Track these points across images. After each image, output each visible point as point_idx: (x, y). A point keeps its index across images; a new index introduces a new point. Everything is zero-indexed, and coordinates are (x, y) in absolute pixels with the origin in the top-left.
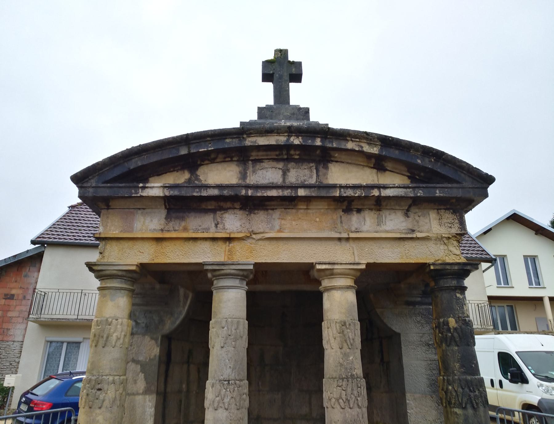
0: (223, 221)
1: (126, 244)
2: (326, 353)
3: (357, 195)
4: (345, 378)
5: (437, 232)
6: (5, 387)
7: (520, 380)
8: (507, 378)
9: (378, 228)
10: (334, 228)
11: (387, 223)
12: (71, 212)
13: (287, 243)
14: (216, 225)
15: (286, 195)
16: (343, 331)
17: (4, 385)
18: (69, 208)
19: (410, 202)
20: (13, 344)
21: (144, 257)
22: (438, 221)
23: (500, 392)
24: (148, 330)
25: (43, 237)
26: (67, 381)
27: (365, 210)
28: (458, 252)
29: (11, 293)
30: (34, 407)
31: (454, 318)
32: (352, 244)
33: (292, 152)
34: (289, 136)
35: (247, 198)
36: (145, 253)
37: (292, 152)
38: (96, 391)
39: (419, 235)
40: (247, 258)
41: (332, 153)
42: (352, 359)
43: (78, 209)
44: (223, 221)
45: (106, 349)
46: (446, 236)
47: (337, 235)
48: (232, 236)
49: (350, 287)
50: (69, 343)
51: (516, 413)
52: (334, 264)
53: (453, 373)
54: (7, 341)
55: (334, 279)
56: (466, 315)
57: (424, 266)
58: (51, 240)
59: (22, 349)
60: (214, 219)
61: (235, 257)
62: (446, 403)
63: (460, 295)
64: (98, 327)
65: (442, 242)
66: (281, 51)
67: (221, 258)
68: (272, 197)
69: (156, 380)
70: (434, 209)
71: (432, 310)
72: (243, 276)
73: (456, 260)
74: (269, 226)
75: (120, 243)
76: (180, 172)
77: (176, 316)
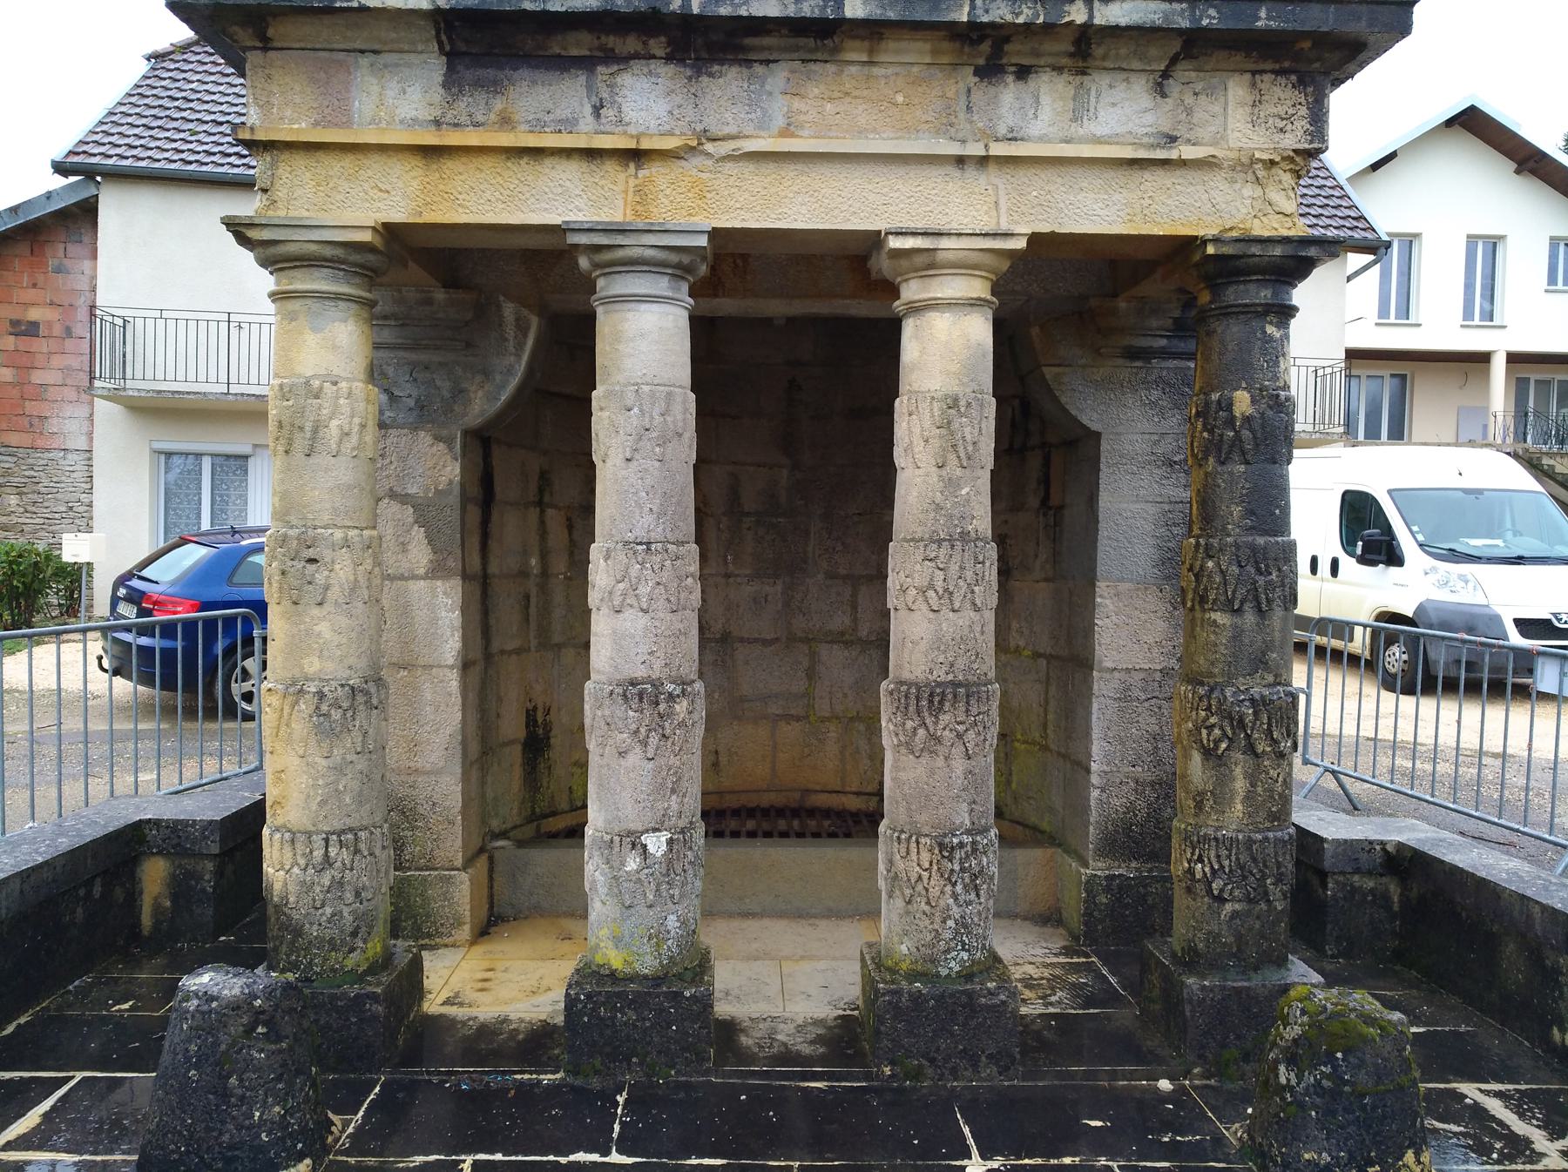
0: (617, 98)
2: (901, 478)
3: (1021, 20)
4: (944, 540)
5: (1241, 145)
6: (67, 563)
7: (1383, 558)
8: (1351, 554)
10: (945, 128)
11: (1102, 113)
12: (157, 73)
13: (806, 169)
14: (597, 110)
15: (808, 15)
16: (949, 423)
17: (64, 560)
18: (148, 59)
19: (1176, 46)
21: (392, 203)
22: (1248, 109)
23: (1331, 586)
24: (424, 415)
25: (84, 152)
26: (226, 549)
27: (1040, 69)
28: (1290, 206)
29: (30, 319)
30: (153, 609)
31: (1249, 392)
32: (993, 176)
36: (393, 193)
38: (303, 563)
39: (1188, 152)
40: (690, 215)
42: (968, 493)
43: (177, 65)
44: (617, 98)
45: (311, 460)
46: (1265, 156)
47: (954, 149)
48: (645, 145)
49: (978, 303)
51: (1358, 630)
52: (940, 234)
53: (1224, 529)
54: (48, 450)
55: (936, 278)
56: (1282, 384)
57: (1188, 245)
58: (110, 162)
59: (92, 472)
60: (590, 88)
61: (655, 210)
62: (1193, 600)
63: (1274, 329)
64: (285, 403)
65: (1250, 177)
67: (614, 213)
68: (765, 19)
69: (459, 542)
70: (1243, 71)
71: (1192, 372)
72: (678, 266)
73: (1280, 230)
74: (753, 116)
75: (318, 162)
77: (498, 377)
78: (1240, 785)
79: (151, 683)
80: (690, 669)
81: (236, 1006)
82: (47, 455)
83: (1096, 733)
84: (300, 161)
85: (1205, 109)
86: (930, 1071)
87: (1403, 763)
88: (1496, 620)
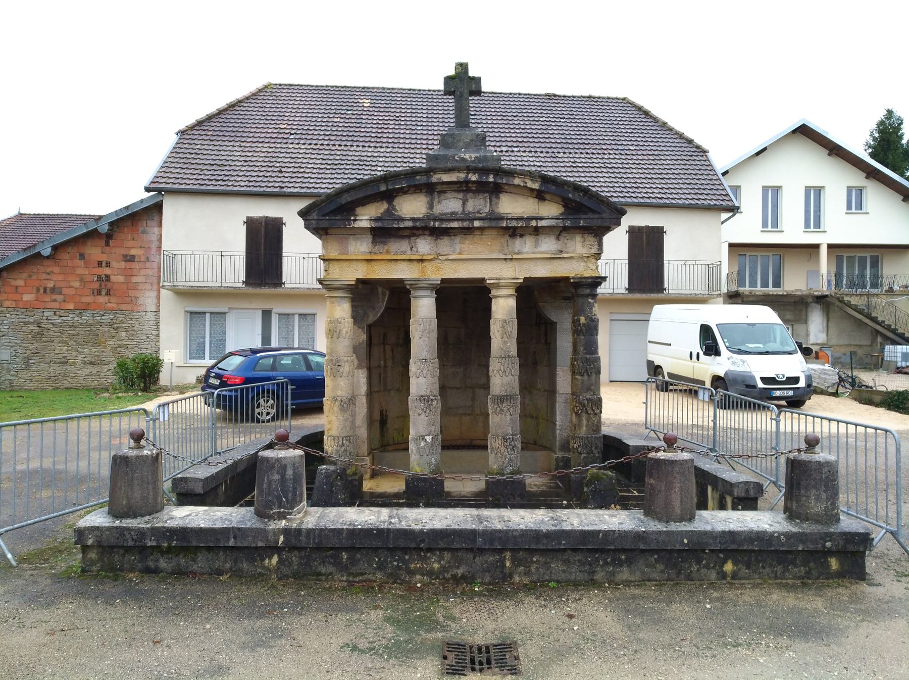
1: (345, 264)
7: (714, 353)
10: (501, 251)
14: (411, 249)
20: (145, 315)
23: (697, 364)
32: (515, 263)
33: (470, 185)
34: (468, 174)
35: (434, 228)
37: (470, 185)
39: (565, 255)
41: (503, 185)
45: (339, 339)
48: (424, 258)
50: (211, 313)
57: (567, 278)
60: (409, 243)
66: (461, 65)
76: (380, 203)
78: (585, 422)
79: (218, 407)
80: (437, 392)
81: (334, 471)
83: (558, 413)
84: (335, 263)
85: (570, 244)
86: (502, 499)
87: (695, 431)
88: (753, 378)
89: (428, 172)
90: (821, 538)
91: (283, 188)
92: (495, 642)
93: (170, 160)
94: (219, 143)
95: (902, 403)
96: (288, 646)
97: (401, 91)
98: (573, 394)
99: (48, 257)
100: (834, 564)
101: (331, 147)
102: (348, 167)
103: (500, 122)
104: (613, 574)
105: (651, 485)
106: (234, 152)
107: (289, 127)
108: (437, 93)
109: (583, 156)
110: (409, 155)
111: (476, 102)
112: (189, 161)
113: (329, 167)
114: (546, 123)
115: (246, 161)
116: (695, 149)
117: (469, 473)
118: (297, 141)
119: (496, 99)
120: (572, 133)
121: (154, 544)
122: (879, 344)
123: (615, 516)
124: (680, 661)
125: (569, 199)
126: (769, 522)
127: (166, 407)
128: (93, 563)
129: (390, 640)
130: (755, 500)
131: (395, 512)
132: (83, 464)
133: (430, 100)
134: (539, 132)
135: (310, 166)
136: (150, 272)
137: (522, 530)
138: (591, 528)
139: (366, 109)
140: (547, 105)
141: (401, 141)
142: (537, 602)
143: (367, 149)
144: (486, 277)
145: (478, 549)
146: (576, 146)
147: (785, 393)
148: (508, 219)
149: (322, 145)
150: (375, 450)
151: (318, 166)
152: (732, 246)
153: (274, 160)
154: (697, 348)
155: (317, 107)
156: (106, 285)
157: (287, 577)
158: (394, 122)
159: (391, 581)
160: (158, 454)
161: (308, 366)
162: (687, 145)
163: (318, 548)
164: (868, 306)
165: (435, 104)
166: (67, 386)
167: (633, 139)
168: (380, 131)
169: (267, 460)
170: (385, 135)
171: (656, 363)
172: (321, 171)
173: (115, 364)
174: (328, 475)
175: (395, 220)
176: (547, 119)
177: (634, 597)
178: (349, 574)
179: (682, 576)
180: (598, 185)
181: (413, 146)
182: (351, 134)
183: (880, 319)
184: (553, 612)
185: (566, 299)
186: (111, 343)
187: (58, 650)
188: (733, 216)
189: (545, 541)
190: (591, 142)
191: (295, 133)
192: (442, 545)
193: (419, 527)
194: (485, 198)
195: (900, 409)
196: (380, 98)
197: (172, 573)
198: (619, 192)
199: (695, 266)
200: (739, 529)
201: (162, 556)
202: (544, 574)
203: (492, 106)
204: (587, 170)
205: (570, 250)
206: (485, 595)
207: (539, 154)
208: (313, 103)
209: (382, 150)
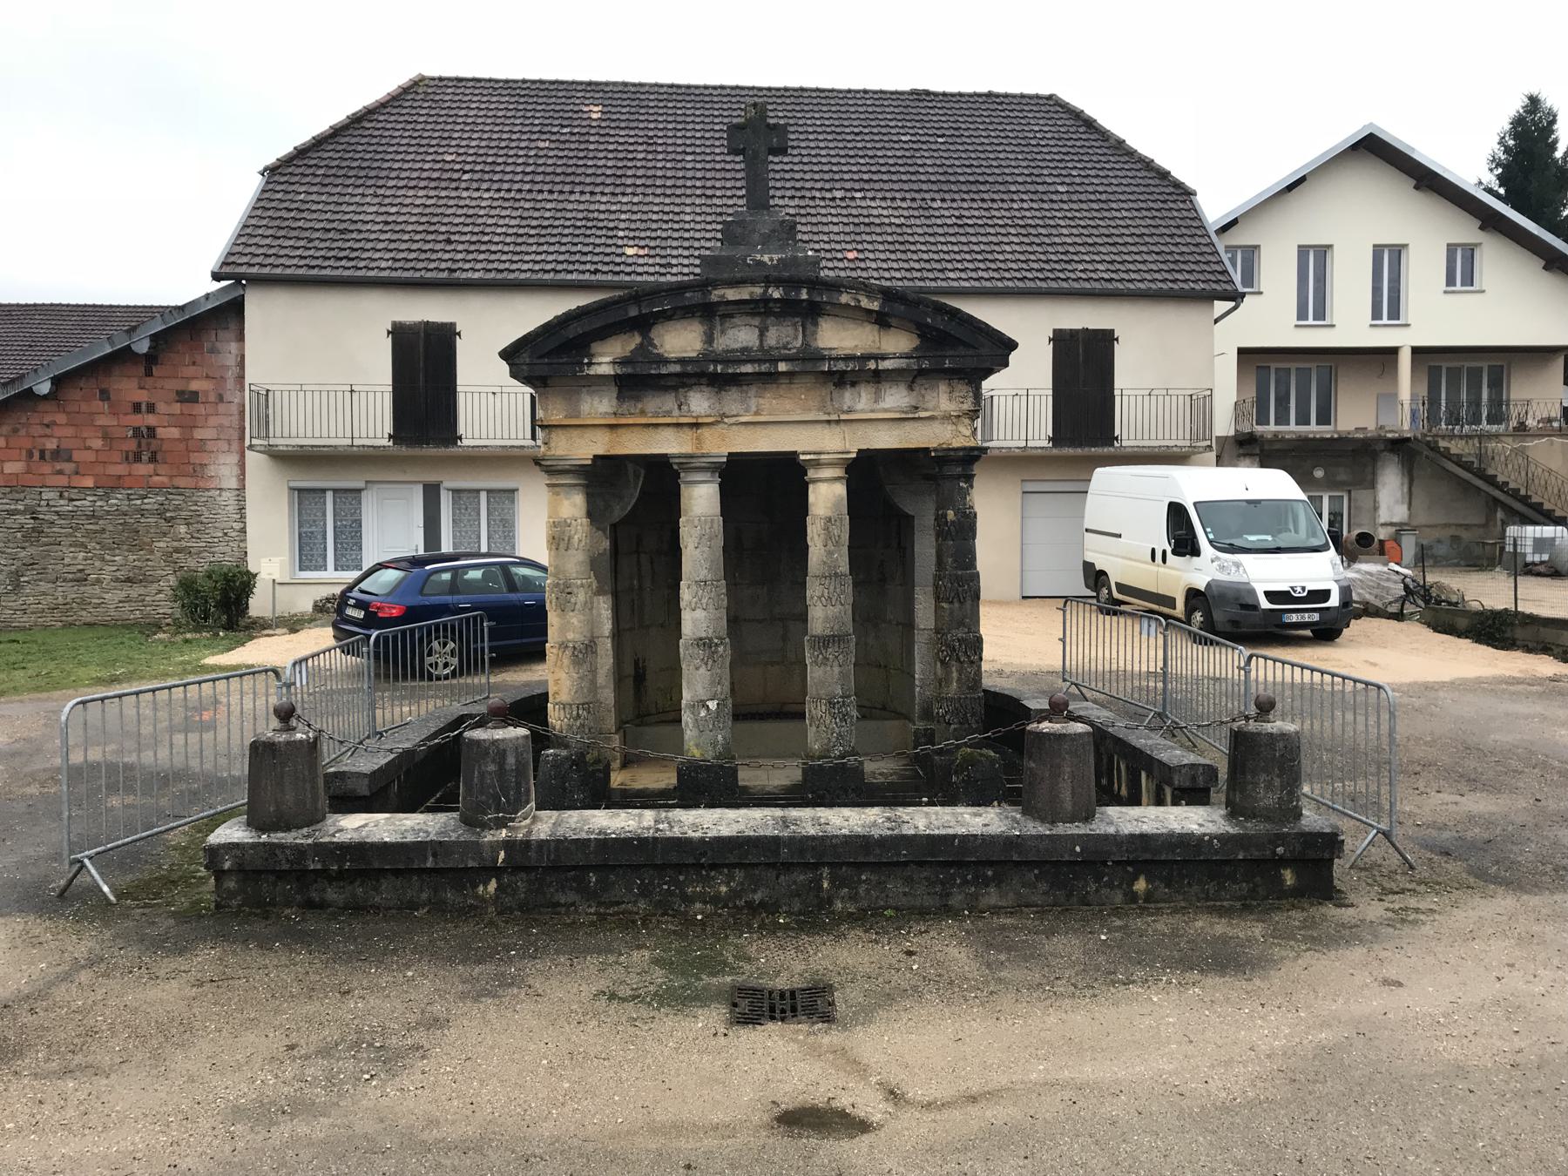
1: (575, 433)
9: (876, 406)
10: (822, 408)
23: (1163, 570)
25: (233, 263)
32: (843, 427)
34: (767, 287)
37: (771, 305)
39: (923, 414)
47: (826, 417)
48: (700, 421)
52: (820, 453)
54: (208, 490)
57: (927, 450)
78: (955, 675)
80: (724, 633)
81: (566, 758)
82: (207, 494)
84: (560, 432)
88: (1252, 592)
89: (704, 285)
90: (1270, 842)
91: (455, 271)
92: (805, 986)
93: (253, 222)
94: (338, 189)
95: (1499, 630)
96: (522, 996)
97: (656, 89)
98: (937, 631)
99: (45, 397)
100: (1288, 877)
101: (534, 195)
102: (566, 231)
103: (831, 145)
104: (976, 896)
105: (1031, 769)
106: (366, 208)
107: (459, 159)
108: (719, 91)
109: (975, 205)
110: (672, 208)
111: (789, 108)
112: (286, 223)
113: (532, 232)
114: (911, 145)
115: (387, 223)
116: (1172, 190)
117: (778, 757)
118: (475, 185)
119: (823, 101)
120: (957, 163)
121: (319, 867)
122: (1499, 523)
123: (980, 815)
124: (1048, 1002)
125: (927, 325)
126: (1200, 821)
127: (304, 665)
128: (232, 894)
129: (660, 986)
130: (1207, 790)
131: (663, 815)
132: (163, 753)
133: (707, 106)
134: (900, 161)
135: (499, 230)
136: (225, 421)
137: (845, 836)
138: (943, 832)
139: (594, 124)
140: (914, 111)
141: (659, 182)
142: (865, 937)
143: (598, 198)
144: (799, 450)
145: (782, 864)
146: (964, 188)
147: (1307, 617)
148: (830, 359)
149: (520, 191)
150: (627, 722)
151: (515, 230)
152: (1243, 352)
153: (435, 220)
154: (1163, 543)
155: (508, 122)
156: (149, 444)
157: (511, 910)
158: (644, 147)
159: (660, 912)
160: (316, 739)
161: (511, 584)
162: (1158, 182)
163: (554, 868)
164: (1480, 457)
165: (716, 113)
166: (88, 620)
167: (1064, 172)
168: (620, 164)
169: (478, 743)
170: (630, 173)
171: (1098, 568)
172: (520, 240)
173: (173, 581)
174: (557, 763)
175: (654, 362)
176: (914, 139)
177: (1003, 928)
178: (600, 904)
179: (1075, 899)
180: (1001, 257)
181: (678, 192)
182: (570, 170)
183: (1500, 479)
184: (887, 948)
185: (927, 478)
186: (162, 544)
187: (215, 1004)
188: (1235, 308)
189: (878, 851)
190: (990, 179)
191: (471, 171)
192: (732, 859)
193: (699, 834)
194: (795, 325)
195: (1497, 640)
196: (619, 102)
197: (345, 908)
198: (1037, 270)
199: (1167, 398)
200: (1155, 831)
201: (330, 884)
202: (877, 897)
203: (817, 115)
204: (982, 231)
205: (930, 405)
206: (793, 928)
207: (899, 203)
208: (500, 114)
209: (625, 200)
